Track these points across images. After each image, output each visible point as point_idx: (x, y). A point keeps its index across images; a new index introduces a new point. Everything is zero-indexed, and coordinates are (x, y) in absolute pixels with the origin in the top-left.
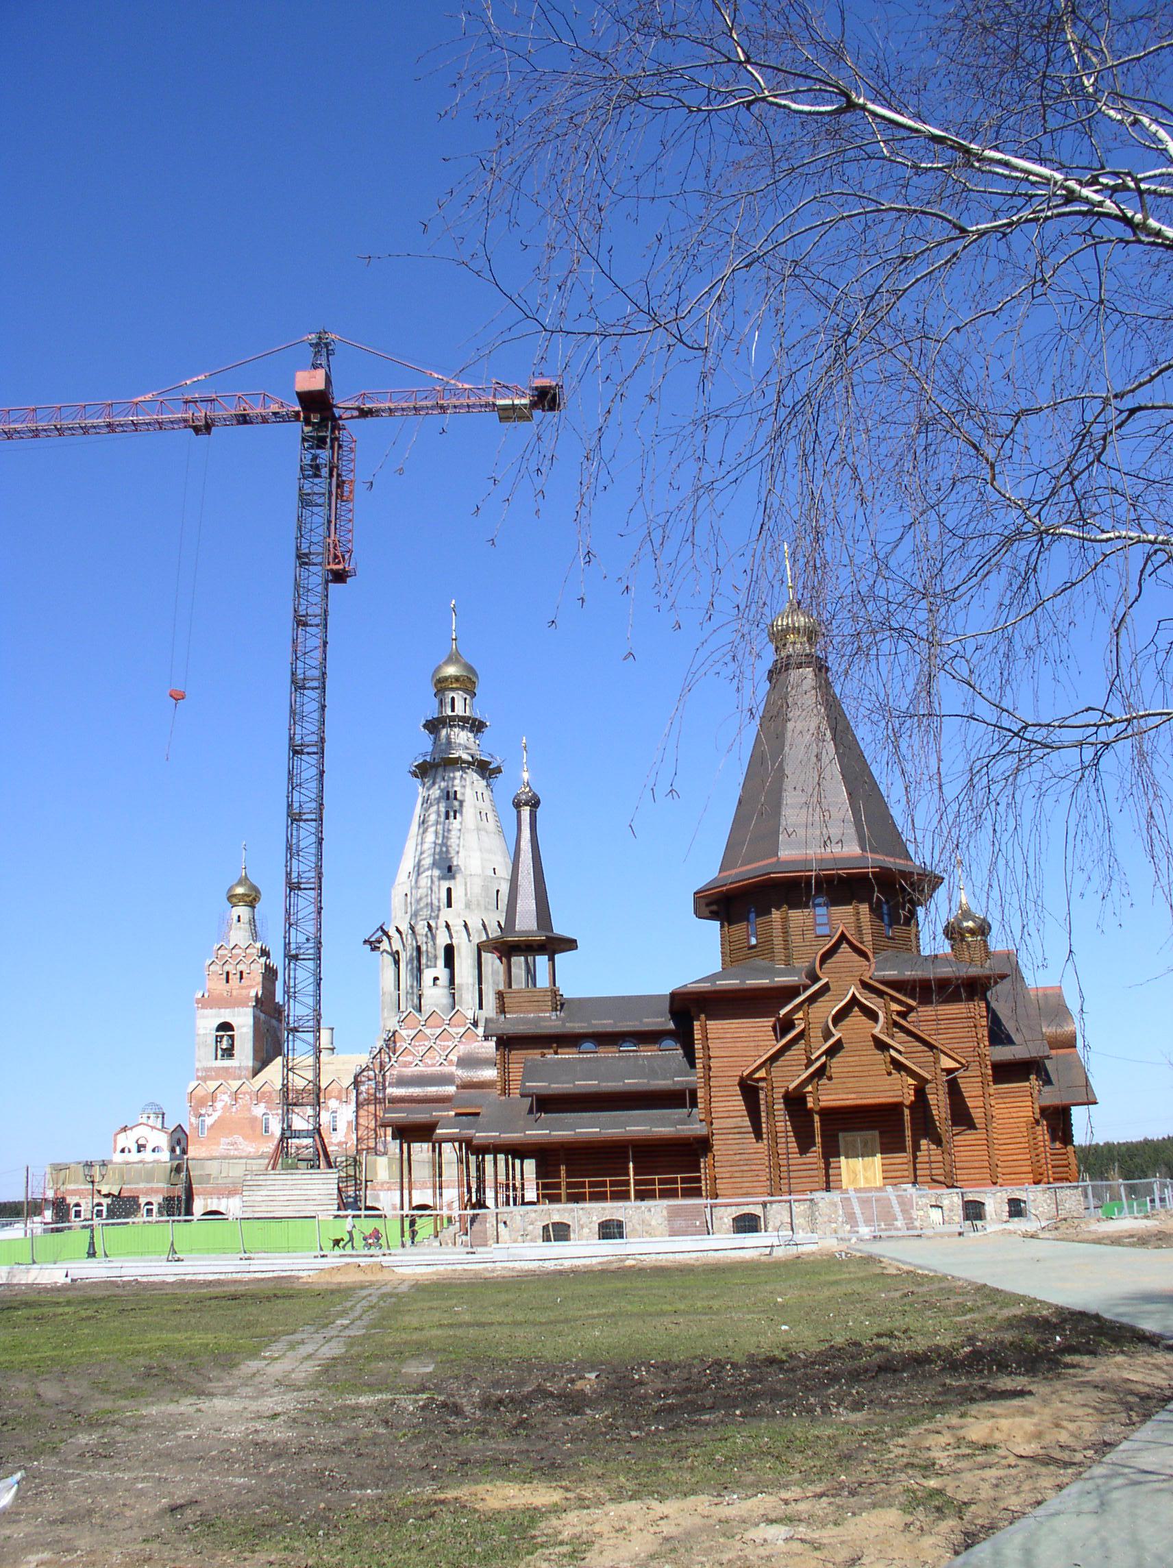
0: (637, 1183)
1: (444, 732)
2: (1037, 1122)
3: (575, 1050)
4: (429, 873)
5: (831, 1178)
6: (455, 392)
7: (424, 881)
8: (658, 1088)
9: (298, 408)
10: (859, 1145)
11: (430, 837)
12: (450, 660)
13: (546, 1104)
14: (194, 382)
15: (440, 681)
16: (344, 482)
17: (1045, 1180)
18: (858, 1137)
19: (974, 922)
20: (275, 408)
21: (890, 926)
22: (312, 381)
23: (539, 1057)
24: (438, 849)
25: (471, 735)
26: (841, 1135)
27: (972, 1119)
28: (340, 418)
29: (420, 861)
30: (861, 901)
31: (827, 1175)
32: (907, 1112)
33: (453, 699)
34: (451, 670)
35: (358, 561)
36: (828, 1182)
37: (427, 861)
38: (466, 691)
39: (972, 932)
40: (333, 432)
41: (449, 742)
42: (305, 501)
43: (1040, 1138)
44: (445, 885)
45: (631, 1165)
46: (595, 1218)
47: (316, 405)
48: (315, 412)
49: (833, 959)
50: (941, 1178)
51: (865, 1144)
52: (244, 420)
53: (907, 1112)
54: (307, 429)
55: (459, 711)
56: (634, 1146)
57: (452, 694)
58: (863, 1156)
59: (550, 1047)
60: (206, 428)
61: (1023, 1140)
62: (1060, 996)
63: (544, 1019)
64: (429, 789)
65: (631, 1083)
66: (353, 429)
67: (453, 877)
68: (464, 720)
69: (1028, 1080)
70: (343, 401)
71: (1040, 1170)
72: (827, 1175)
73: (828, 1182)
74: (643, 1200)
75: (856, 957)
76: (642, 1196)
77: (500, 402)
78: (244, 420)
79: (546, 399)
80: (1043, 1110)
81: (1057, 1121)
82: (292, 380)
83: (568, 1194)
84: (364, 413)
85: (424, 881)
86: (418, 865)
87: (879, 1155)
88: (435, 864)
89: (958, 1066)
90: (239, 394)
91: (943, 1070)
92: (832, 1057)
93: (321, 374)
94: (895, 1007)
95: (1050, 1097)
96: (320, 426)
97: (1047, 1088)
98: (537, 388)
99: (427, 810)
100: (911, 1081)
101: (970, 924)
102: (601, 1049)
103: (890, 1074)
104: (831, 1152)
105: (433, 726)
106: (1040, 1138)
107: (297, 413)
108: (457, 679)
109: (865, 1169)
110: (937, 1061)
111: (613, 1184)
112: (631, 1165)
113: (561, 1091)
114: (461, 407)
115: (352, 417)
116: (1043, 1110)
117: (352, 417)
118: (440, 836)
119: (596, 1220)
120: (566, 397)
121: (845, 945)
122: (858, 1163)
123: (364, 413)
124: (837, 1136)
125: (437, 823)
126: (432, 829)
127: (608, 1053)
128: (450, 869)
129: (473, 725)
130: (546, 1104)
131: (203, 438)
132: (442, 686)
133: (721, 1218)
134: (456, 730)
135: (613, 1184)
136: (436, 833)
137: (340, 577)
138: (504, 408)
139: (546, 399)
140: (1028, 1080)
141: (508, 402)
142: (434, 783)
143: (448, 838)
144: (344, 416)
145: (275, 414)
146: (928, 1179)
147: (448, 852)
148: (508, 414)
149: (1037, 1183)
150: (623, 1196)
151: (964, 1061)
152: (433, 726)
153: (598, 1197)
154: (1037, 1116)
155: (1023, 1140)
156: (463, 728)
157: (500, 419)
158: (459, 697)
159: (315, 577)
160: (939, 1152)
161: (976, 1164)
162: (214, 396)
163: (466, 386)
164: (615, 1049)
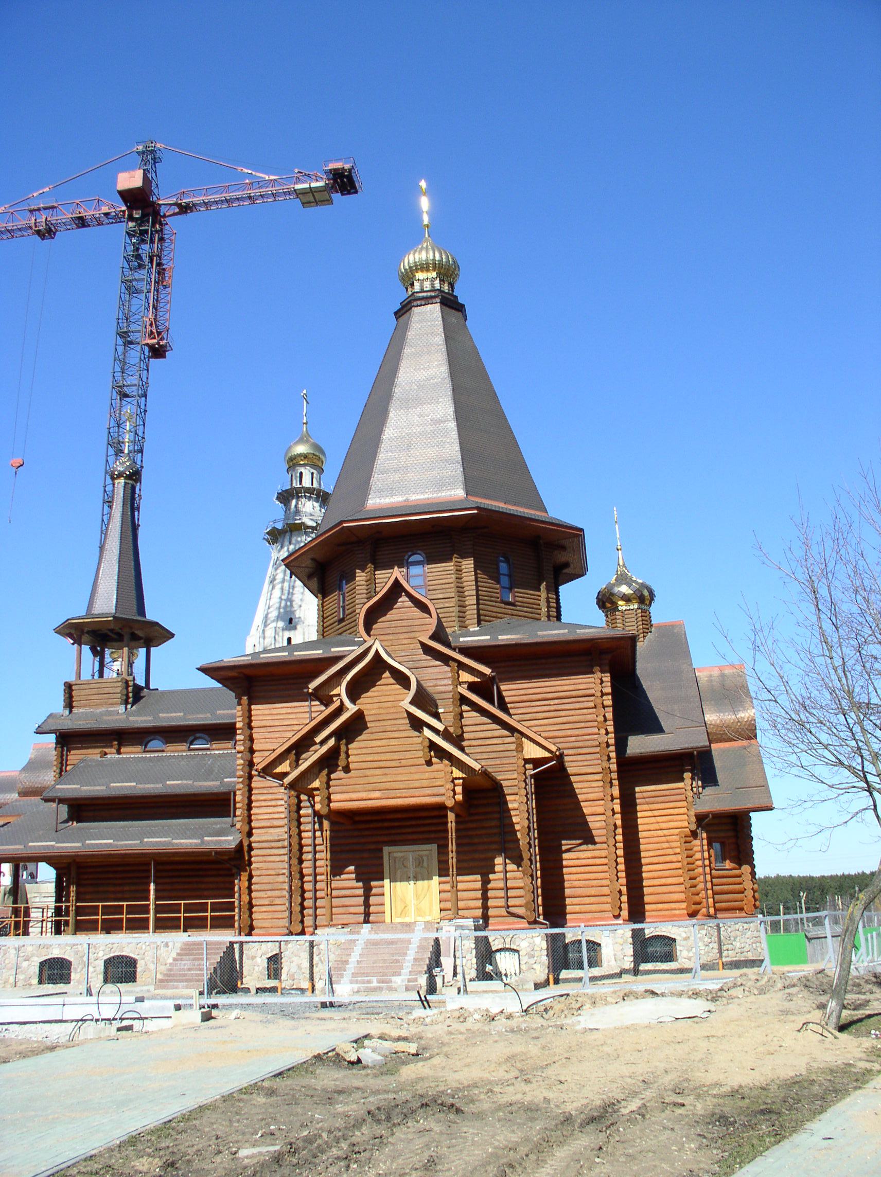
0: (158, 909)
1: (294, 502)
2: (694, 834)
3: (139, 748)
4: (274, 625)
5: (372, 909)
6: (261, 183)
7: (270, 632)
8: (204, 790)
9: (124, 208)
10: (411, 863)
11: (277, 593)
12: (301, 441)
13: (83, 810)
14: (40, 195)
15: (292, 459)
16: (164, 270)
17: (704, 910)
18: (407, 853)
19: (629, 586)
20: (105, 209)
21: (510, 589)
22: (132, 179)
23: (98, 757)
24: (283, 604)
25: (317, 505)
26: (386, 849)
27: (590, 830)
28: (165, 216)
29: (267, 614)
30: (463, 556)
31: (367, 905)
32: (451, 816)
33: (301, 474)
34: (301, 449)
35: (175, 339)
36: (367, 914)
37: (273, 614)
38: (313, 466)
39: (627, 599)
40: (153, 225)
41: (297, 511)
42: (131, 289)
43: (698, 856)
44: (287, 634)
45: (152, 887)
46: (101, 954)
47: (139, 201)
48: (137, 209)
49: (388, 617)
50: (521, 911)
51: (419, 862)
52: (82, 222)
53: (451, 816)
54: (131, 224)
55: (306, 483)
56: (157, 863)
57: (302, 469)
58: (416, 879)
59: (111, 747)
60: (47, 233)
61: (674, 858)
62: (742, 676)
63: (109, 713)
64: (279, 551)
65: (176, 784)
66: (174, 225)
67: (295, 628)
68: (310, 491)
69: (682, 780)
70: (164, 198)
71: (697, 898)
72: (367, 905)
73: (367, 914)
74: (108, 933)
75: (417, 612)
76: (163, 925)
77: (299, 186)
78: (82, 222)
79: (343, 182)
80: (701, 819)
81: (730, 835)
82: (115, 183)
83: (157, 920)
84: (184, 209)
85: (270, 632)
86: (266, 617)
87: (436, 879)
88: (278, 618)
89: (547, 755)
90: (77, 201)
91: (527, 761)
92: (350, 741)
93: (139, 174)
94: (466, 677)
95: (714, 800)
96: (141, 221)
97: (709, 790)
98: (331, 170)
99: (276, 569)
100: (457, 773)
101: (624, 589)
102: (170, 747)
103: (429, 763)
104: (371, 874)
105: (285, 497)
106: (698, 856)
107: (124, 212)
108: (305, 456)
109: (417, 896)
110: (520, 748)
111: (131, 909)
112: (152, 887)
113: (93, 794)
114: (268, 196)
115: (174, 214)
116: (701, 819)
117: (174, 214)
118: (286, 592)
119: (103, 955)
120: (360, 178)
121: (404, 598)
122: (400, 886)
123: (184, 209)
124: (381, 850)
125: (283, 581)
126: (279, 586)
127: (177, 751)
128: (291, 621)
129: (318, 495)
130: (83, 810)
131: (47, 242)
132: (293, 462)
133: (253, 958)
134: (303, 500)
135: (131, 909)
136: (282, 589)
137: (158, 352)
138: (303, 192)
139: (343, 182)
140: (682, 780)
141: (306, 186)
142: (282, 547)
143: (293, 594)
144: (168, 214)
145: (106, 214)
146: (503, 912)
147: (291, 605)
148: (311, 198)
149: (693, 915)
150: (139, 925)
151: (554, 748)
152: (285, 497)
153: (110, 927)
154: (693, 827)
155: (674, 858)
156: (310, 498)
157: (303, 204)
158: (307, 472)
159: (134, 355)
160: (519, 874)
161: (593, 891)
162: (55, 205)
163: (272, 177)
164: (184, 747)
